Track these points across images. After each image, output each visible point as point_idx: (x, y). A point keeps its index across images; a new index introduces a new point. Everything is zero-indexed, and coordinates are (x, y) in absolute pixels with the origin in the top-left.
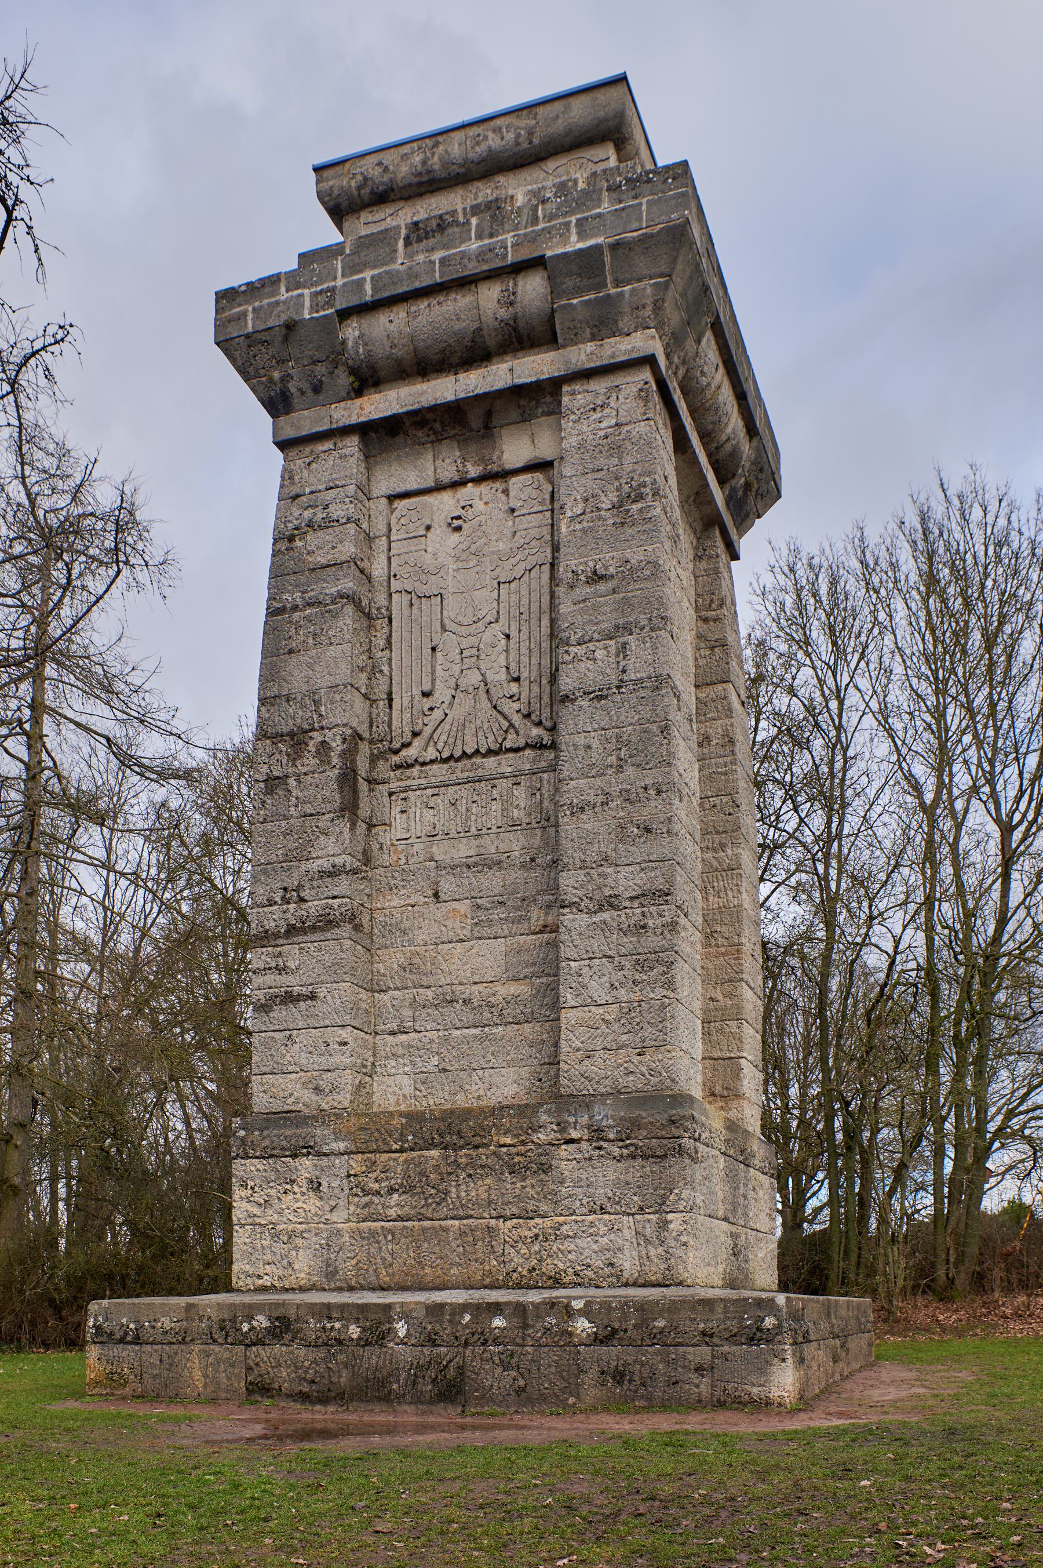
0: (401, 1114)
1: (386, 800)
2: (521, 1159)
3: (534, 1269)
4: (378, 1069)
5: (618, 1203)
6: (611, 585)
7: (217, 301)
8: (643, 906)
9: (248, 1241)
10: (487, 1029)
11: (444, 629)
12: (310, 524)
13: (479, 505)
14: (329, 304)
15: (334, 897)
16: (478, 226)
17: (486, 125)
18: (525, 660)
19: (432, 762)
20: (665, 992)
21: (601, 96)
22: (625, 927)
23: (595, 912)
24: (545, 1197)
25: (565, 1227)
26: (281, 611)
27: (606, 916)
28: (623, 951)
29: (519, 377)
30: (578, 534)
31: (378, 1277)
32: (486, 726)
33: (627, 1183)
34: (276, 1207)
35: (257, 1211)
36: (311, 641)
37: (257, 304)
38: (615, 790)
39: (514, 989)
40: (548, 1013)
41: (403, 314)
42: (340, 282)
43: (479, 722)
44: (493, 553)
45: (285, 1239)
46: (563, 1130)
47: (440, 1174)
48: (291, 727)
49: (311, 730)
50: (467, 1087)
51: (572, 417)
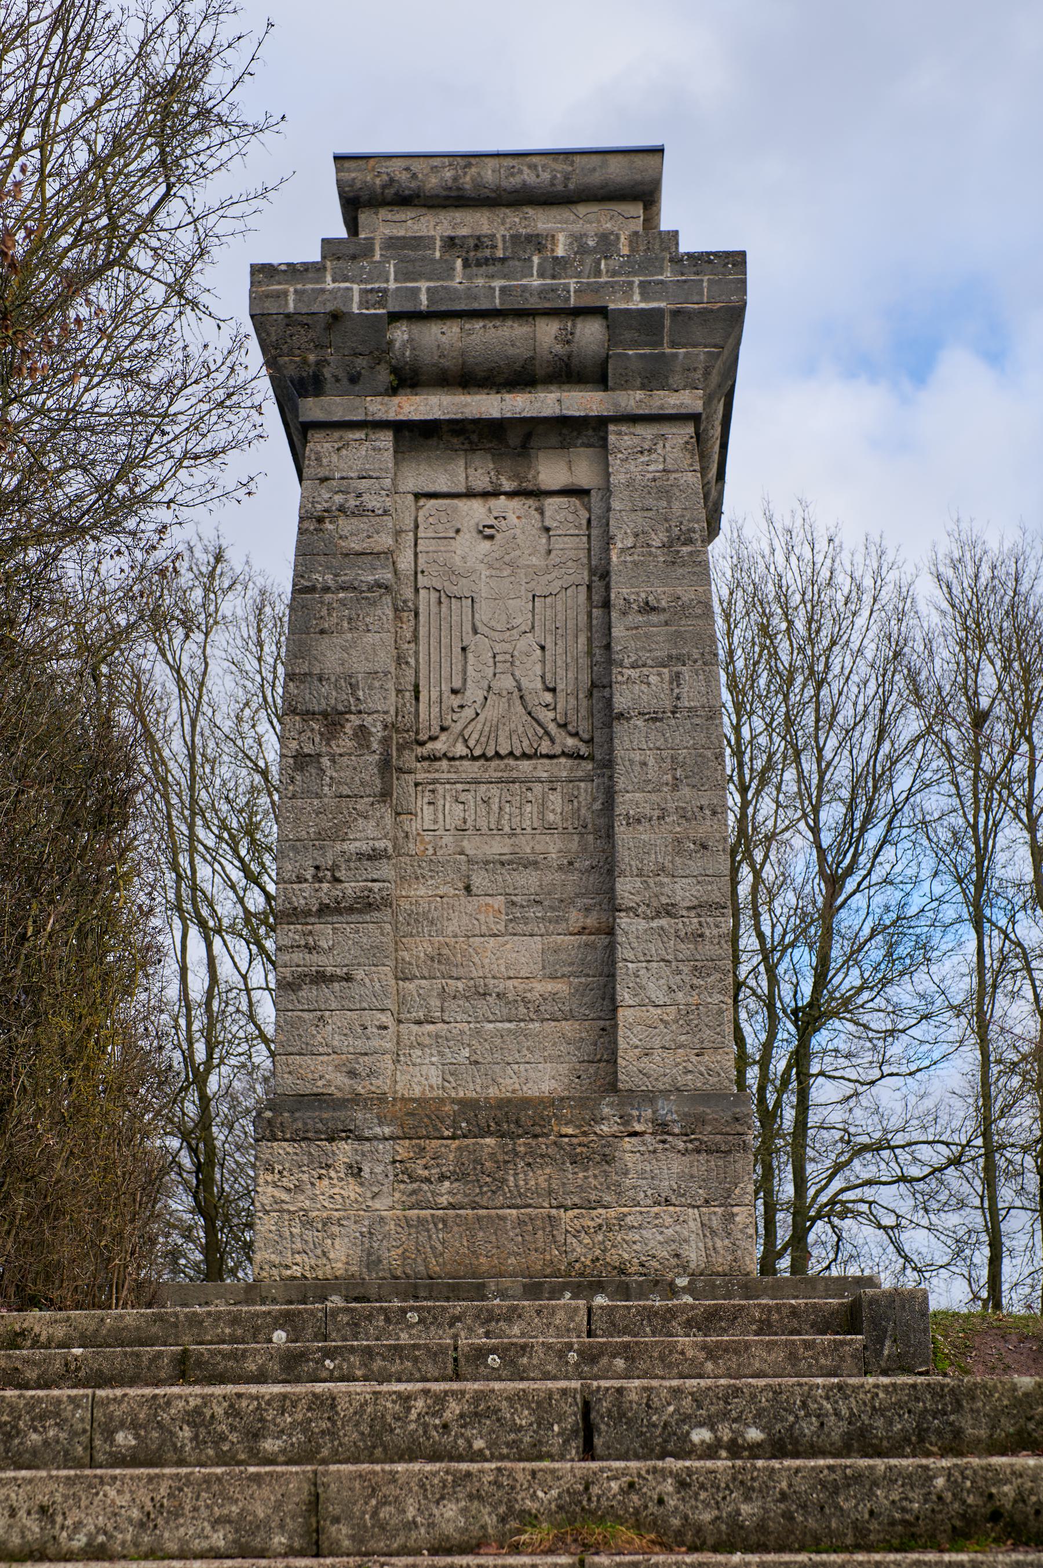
0: (453, 1101)
1: (412, 789)
2: (585, 1150)
3: (598, 1259)
4: (402, 1058)
5: (683, 1195)
6: (663, 617)
7: (252, 274)
8: (700, 916)
9: (273, 1228)
10: (522, 1024)
11: (475, 632)
12: (342, 509)
13: (512, 518)
14: (381, 303)
15: (374, 881)
16: (539, 264)
17: (520, 159)
18: (561, 672)
19: (461, 758)
20: (722, 998)
21: (639, 160)
22: (682, 934)
23: (652, 919)
24: (608, 1188)
25: (629, 1218)
26: (312, 589)
27: (664, 922)
28: (681, 956)
29: (568, 409)
30: (629, 565)
31: (427, 1267)
32: (521, 730)
33: (692, 1176)
34: (309, 1193)
35: (285, 1196)
36: (345, 624)
37: (299, 286)
38: (671, 806)
39: (550, 986)
40: (587, 1012)
41: (456, 329)
42: (392, 285)
43: (513, 726)
44: (528, 566)
45: (320, 1226)
46: (626, 1123)
47: (497, 1162)
48: (324, 706)
49: (346, 713)
50: (501, 1081)
51: (619, 455)
